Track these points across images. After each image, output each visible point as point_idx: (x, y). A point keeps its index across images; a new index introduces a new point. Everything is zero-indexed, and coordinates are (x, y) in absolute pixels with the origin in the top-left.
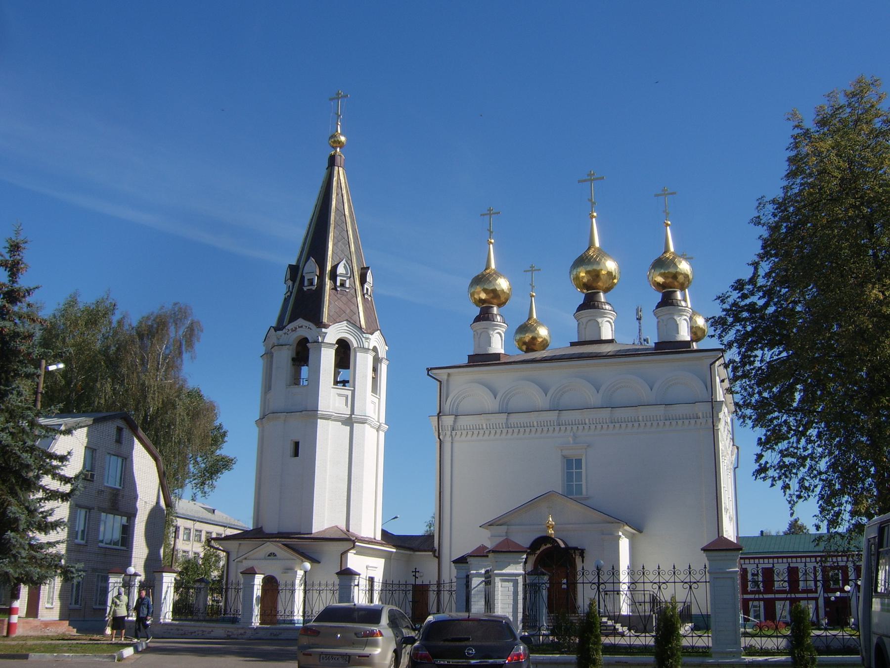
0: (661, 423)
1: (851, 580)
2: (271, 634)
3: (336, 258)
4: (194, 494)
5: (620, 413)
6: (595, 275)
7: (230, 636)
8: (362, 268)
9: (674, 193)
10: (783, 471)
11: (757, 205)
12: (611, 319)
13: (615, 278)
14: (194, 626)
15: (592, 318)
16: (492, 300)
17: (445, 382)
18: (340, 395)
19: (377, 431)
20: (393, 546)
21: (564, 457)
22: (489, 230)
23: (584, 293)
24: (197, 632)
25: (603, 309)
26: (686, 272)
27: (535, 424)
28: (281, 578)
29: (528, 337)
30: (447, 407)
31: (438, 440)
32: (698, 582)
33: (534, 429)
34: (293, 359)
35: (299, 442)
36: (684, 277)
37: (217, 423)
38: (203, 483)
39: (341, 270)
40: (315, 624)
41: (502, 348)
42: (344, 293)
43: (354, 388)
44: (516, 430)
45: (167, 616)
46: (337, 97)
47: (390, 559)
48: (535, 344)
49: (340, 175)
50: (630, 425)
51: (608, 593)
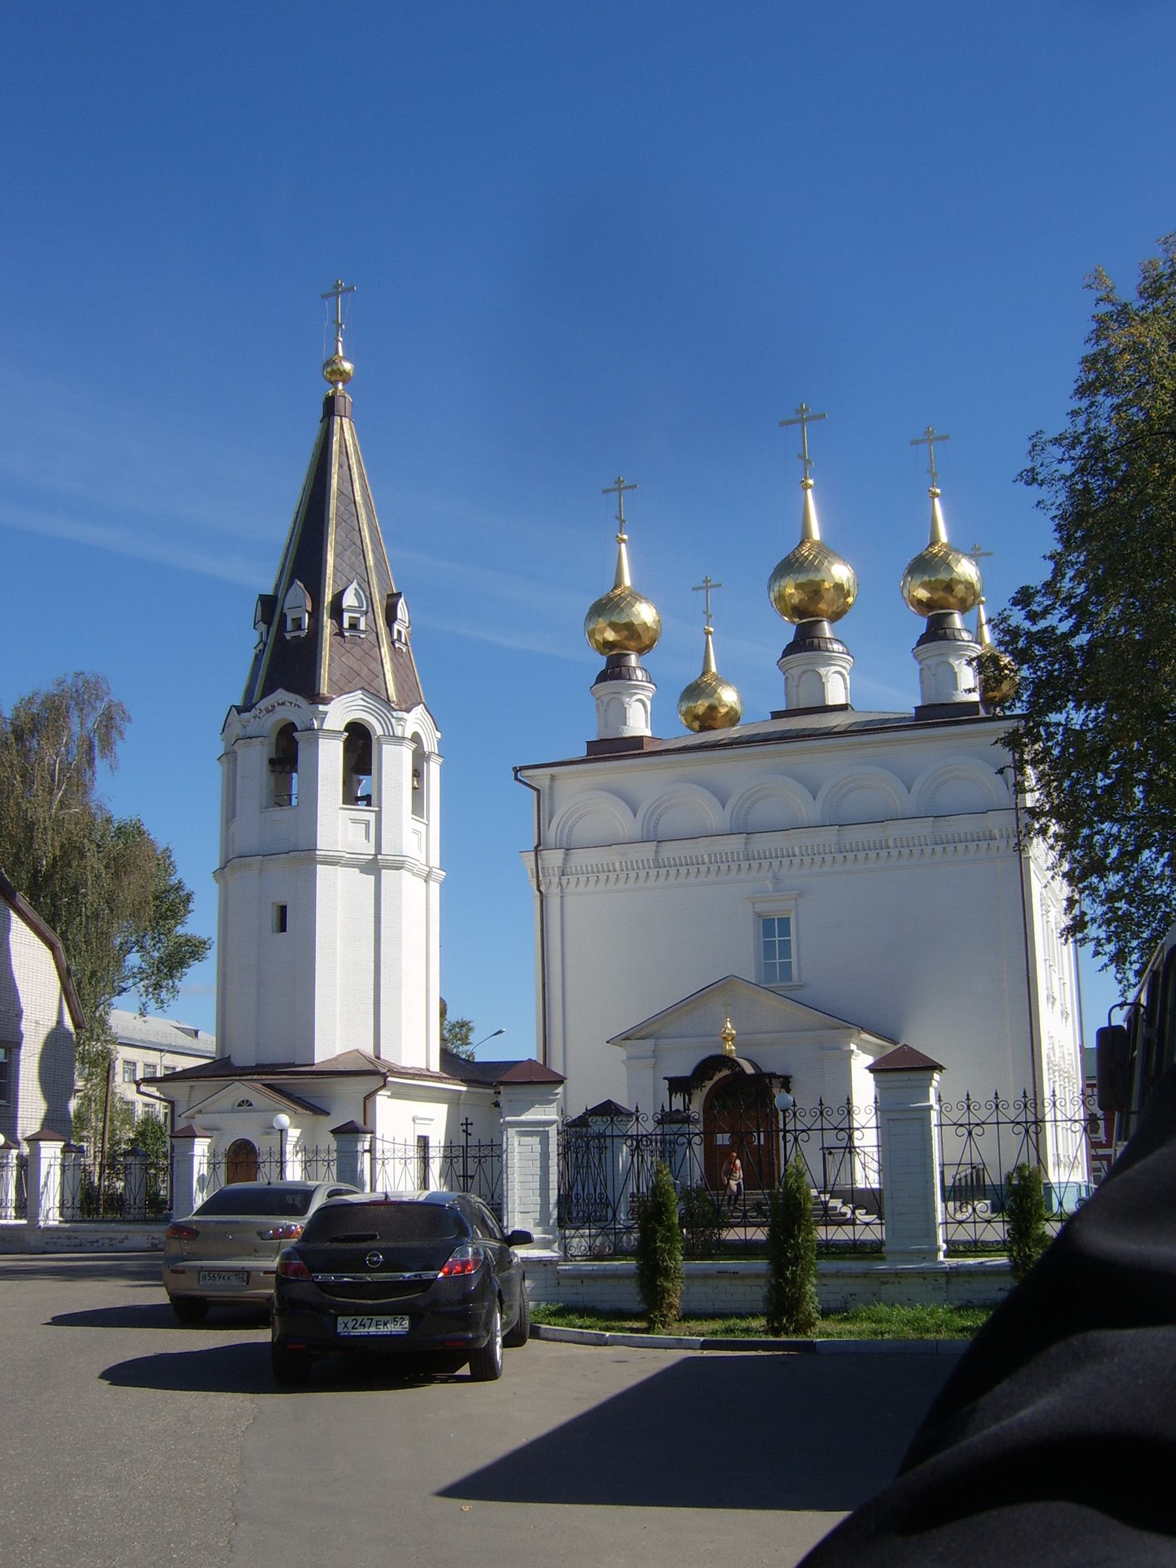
0: (928, 850)
3: (341, 579)
4: (144, 1005)
5: (855, 835)
6: (814, 591)
7: (156, 1245)
8: (388, 596)
9: (947, 437)
10: (1112, 929)
11: (1029, 447)
12: (844, 667)
13: (848, 594)
14: (96, 1231)
15: (810, 667)
16: (626, 643)
17: (547, 791)
18: (354, 821)
19: (426, 881)
20: (461, 1081)
21: (758, 915)
22: (619, 518)
24: (101, 1242)
25: (828, 650)
26: (969, 578)
27: (706, 859)
28: (262, 1144)
29: (701, 706)
30: (551, 835)
31: (538, 893)
32: (983, 1123)
33: (703, 869)
34: (272, 762)
35: (286, 907)
36: (966, 588)
37: (174, 881)
38: (157, 986)
39: (349, 600)
40: (196, 1218)
41: (647, 727)
42: (356, 641)
43: (380, 807)
44: (673, 871)
45: (51, 1216)
46: (336, 292)
47: (458, 1104)
48: (715, 719)
49: (345, 431)
50: (872, 854)
51: (833, 1151)
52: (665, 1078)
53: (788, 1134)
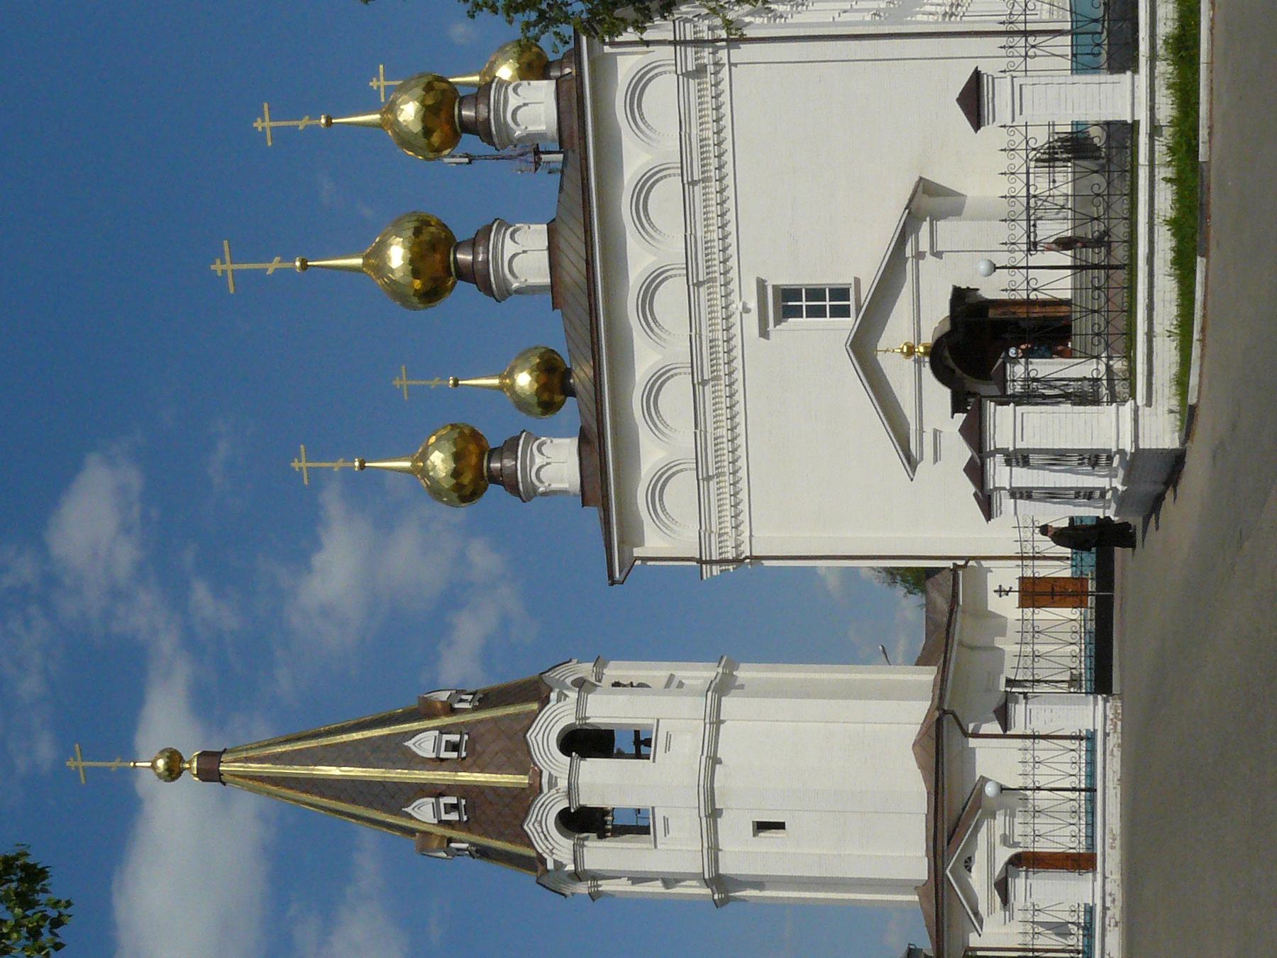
1: (1028, 296)
2: (1112, 848)
23: (454, 283)
32: (1026, 138)
52: (952, 417)
53: (1029, 54)
